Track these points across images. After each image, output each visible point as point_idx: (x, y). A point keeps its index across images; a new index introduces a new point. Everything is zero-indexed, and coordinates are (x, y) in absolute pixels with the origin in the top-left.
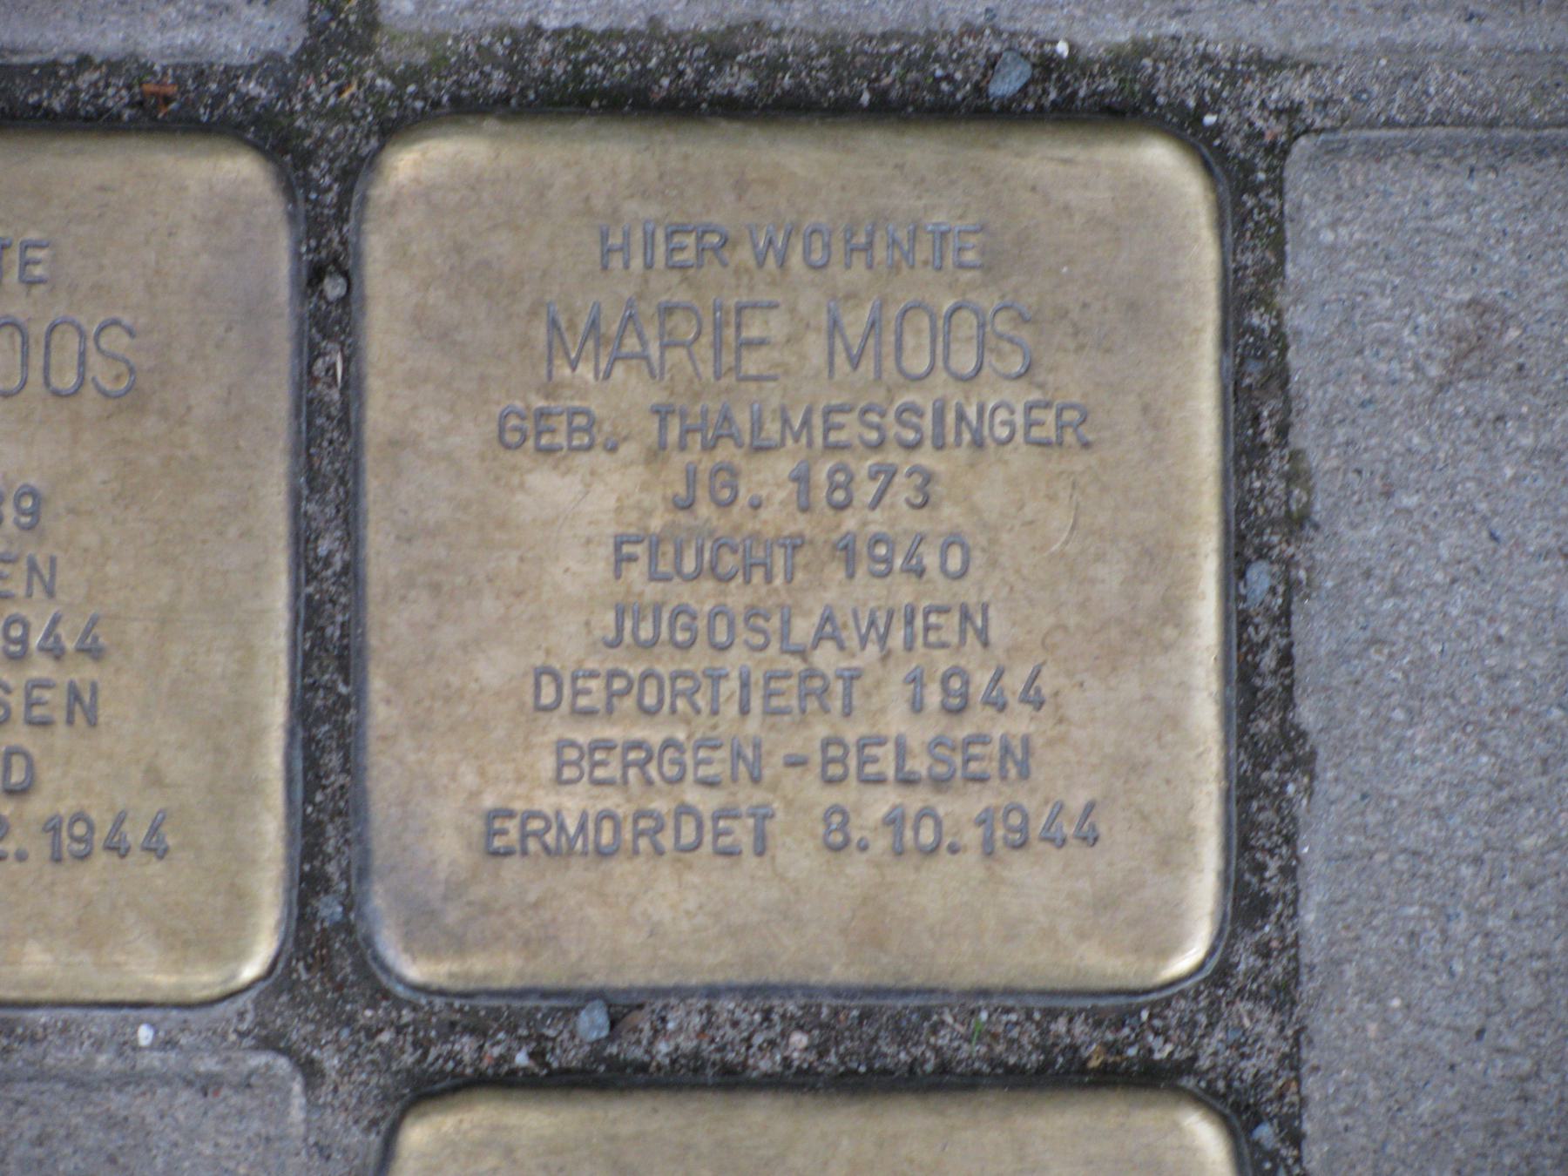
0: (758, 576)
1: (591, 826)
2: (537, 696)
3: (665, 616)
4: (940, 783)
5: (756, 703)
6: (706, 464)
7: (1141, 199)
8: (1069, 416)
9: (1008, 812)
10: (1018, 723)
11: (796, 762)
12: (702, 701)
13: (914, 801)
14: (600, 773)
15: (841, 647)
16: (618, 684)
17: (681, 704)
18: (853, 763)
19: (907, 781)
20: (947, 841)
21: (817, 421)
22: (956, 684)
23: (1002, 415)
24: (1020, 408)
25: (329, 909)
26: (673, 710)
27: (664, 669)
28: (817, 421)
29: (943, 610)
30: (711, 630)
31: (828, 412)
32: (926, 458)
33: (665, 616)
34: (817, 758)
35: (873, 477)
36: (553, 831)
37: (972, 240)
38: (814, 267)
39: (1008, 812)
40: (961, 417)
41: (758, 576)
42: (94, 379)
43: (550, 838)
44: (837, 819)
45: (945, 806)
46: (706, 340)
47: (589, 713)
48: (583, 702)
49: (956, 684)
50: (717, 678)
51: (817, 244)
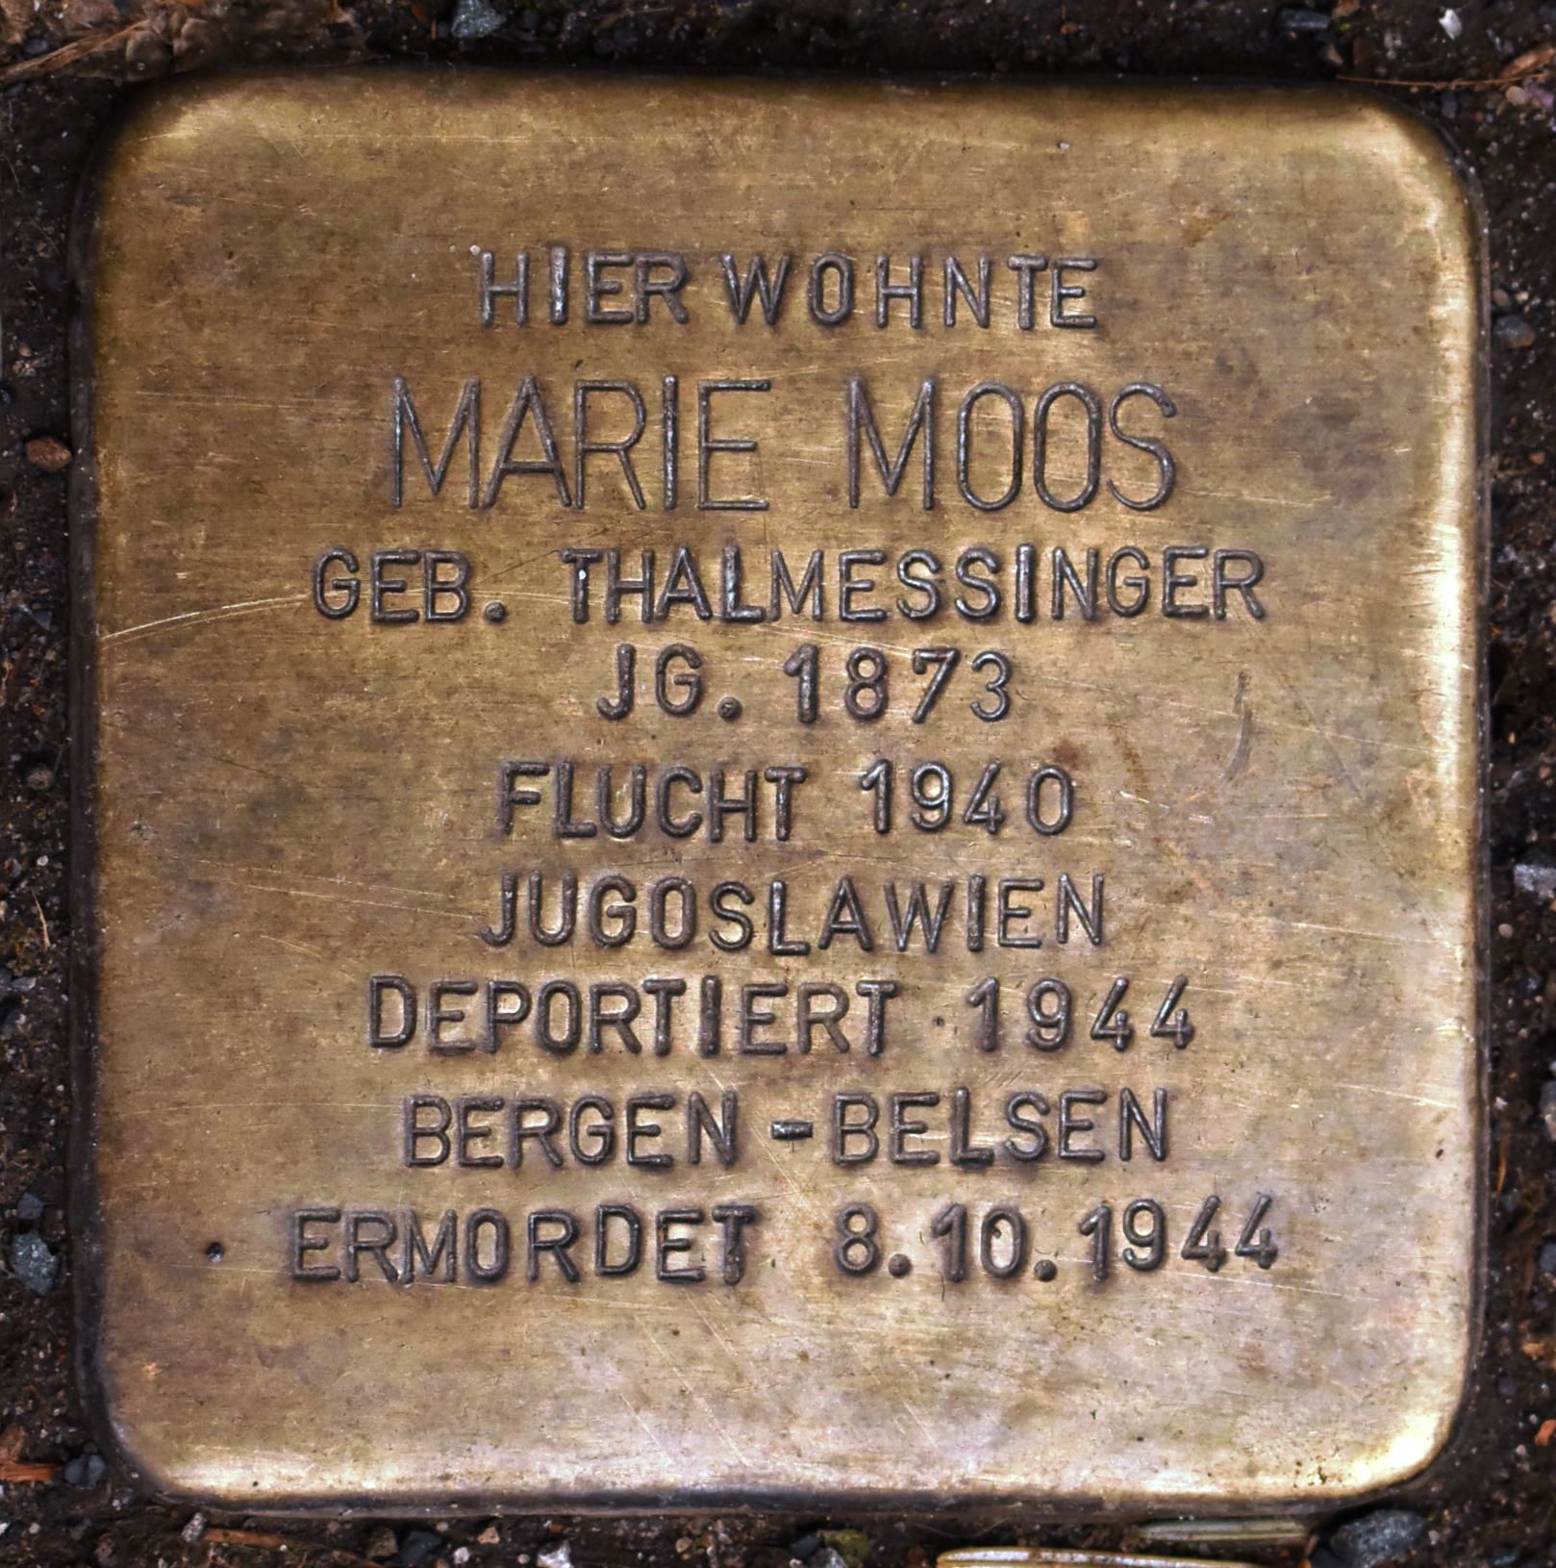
0: (736, 827)
1: (461, 1227)
2: (377, 1021)
3: (584, 896)
4: (1028, 1165)
5: (731, 1035)
6: (649, 647)
7: (1338, 233)
8: (1235, 571)
9: (1133, 1212)
10: (1148, 1073)
11: (797, 1134)
12: (645, 1028)
13: (982, 1195)
14: (478, 1150)
15: (870, 947)
16: (510, 1005)
17: (613, 1038)
18: (884, 1132)
19: (975, 1162)
20: (1036, 1258)
21: (832, 582)
22: (1051, 1005)
23: (1130, 569)
24: (1157, 560)
25: (509, 895)
26: (598, 1048)
27: (586, 982)
28: (832, 582)
29: (1099, 1099)
30: (660, 917)
31: (439, 992)
32: (1005, 638)
33: (584, 896)
34: (823, 1131)
35: (920, 667)
36: (400, 1245)
37: (1085, 280)
38: (830, 325)
39: (1133, 1212)
40: (1062, 567)
41: (736, 827)
42: (1110, 484)
43: (396, 1256)
44: (859, 1225)
45: (1034, 1202)
46: (653, 435)
47: (461, 1052)
48: (451, 1034)
49: (1051, 1005)
50: (669, 992)
51: (833, 281)
